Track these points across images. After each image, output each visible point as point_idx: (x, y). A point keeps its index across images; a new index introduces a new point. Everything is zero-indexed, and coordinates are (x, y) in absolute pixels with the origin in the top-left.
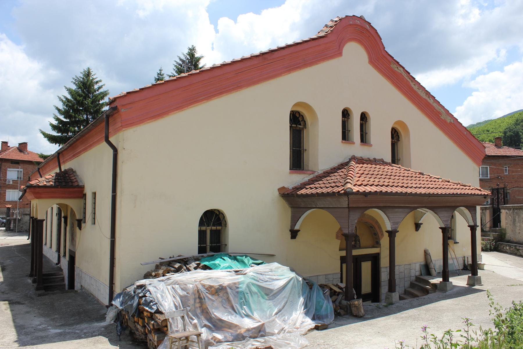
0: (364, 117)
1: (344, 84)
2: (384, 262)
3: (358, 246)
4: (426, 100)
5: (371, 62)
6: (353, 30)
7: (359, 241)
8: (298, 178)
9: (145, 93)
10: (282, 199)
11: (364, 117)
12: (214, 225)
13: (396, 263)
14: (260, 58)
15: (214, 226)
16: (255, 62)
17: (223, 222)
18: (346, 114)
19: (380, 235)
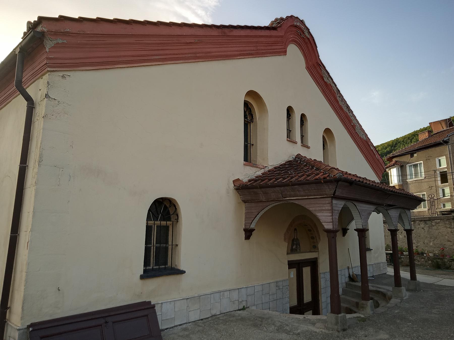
0: (303, 117)
1: (278, 79)
2: (324, 267)
3: (298, 250)
4: (347, 113)
5: (308, 68)
6: (290, 34)
7: (299, 245)
8: (440, 158)
9: (135, 26)
10: (235, 191)
11: (303, 117)
12: (160, 220)
13: (368, 263)
14: (220, 30)
15: (164, 220)
16: (215, 32)
17: (173, 218)
18: (290, 111)
19: (318, 238)
